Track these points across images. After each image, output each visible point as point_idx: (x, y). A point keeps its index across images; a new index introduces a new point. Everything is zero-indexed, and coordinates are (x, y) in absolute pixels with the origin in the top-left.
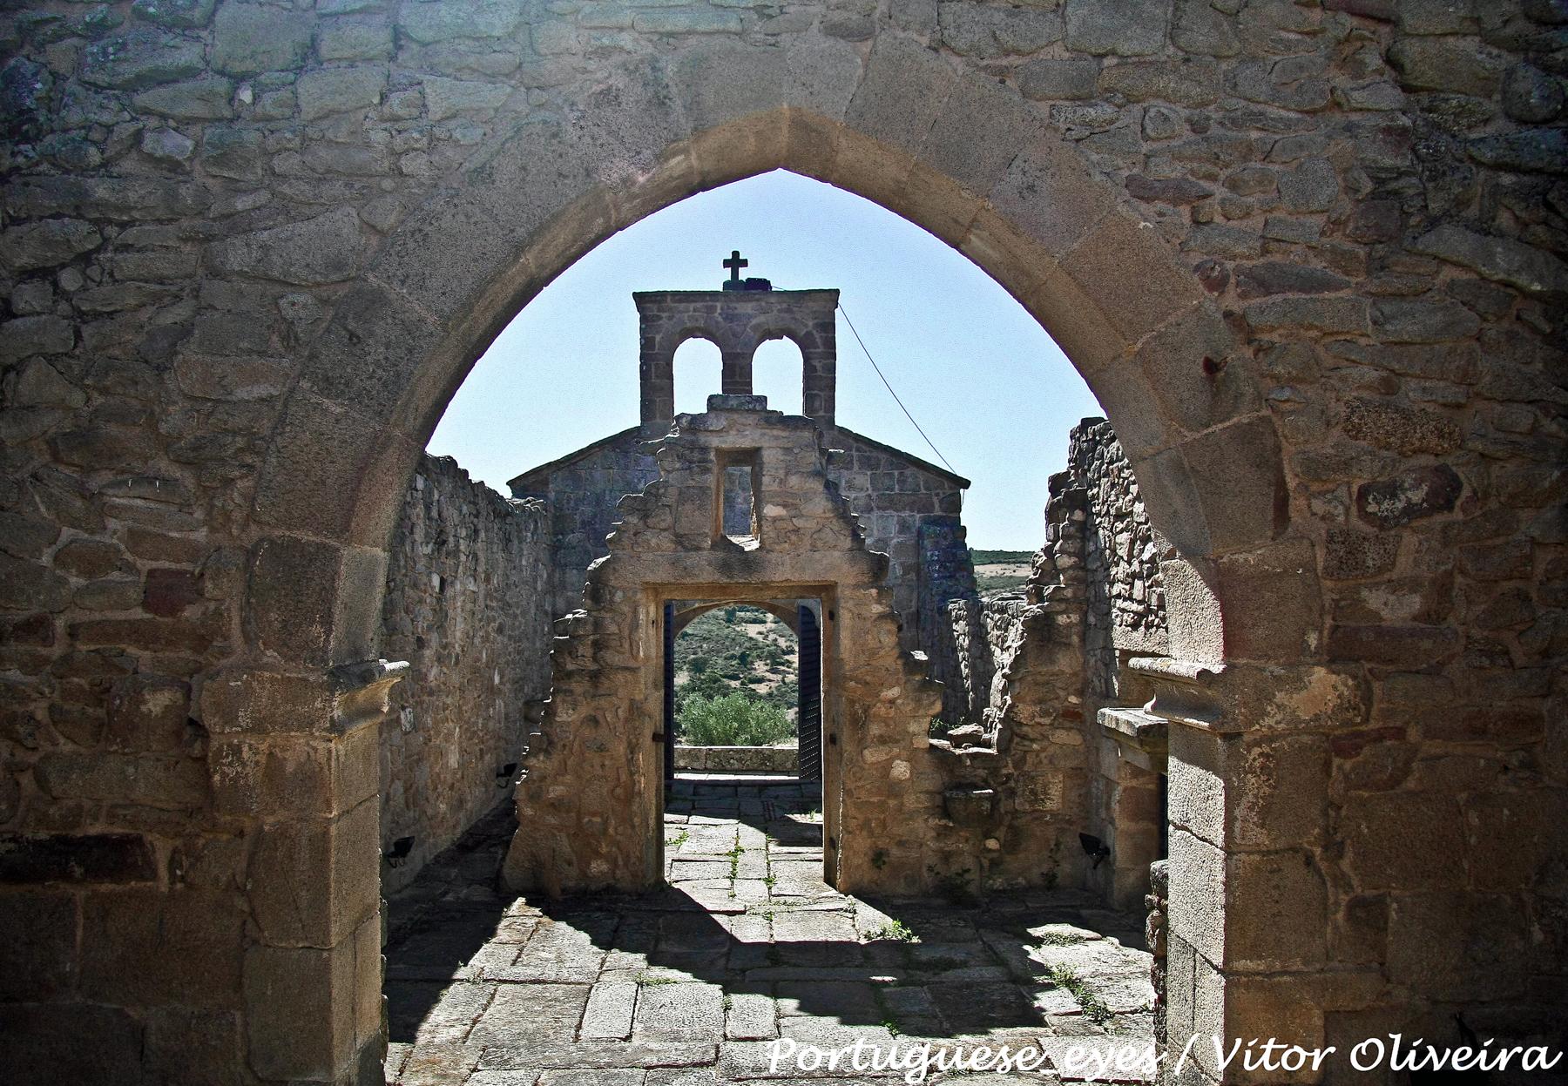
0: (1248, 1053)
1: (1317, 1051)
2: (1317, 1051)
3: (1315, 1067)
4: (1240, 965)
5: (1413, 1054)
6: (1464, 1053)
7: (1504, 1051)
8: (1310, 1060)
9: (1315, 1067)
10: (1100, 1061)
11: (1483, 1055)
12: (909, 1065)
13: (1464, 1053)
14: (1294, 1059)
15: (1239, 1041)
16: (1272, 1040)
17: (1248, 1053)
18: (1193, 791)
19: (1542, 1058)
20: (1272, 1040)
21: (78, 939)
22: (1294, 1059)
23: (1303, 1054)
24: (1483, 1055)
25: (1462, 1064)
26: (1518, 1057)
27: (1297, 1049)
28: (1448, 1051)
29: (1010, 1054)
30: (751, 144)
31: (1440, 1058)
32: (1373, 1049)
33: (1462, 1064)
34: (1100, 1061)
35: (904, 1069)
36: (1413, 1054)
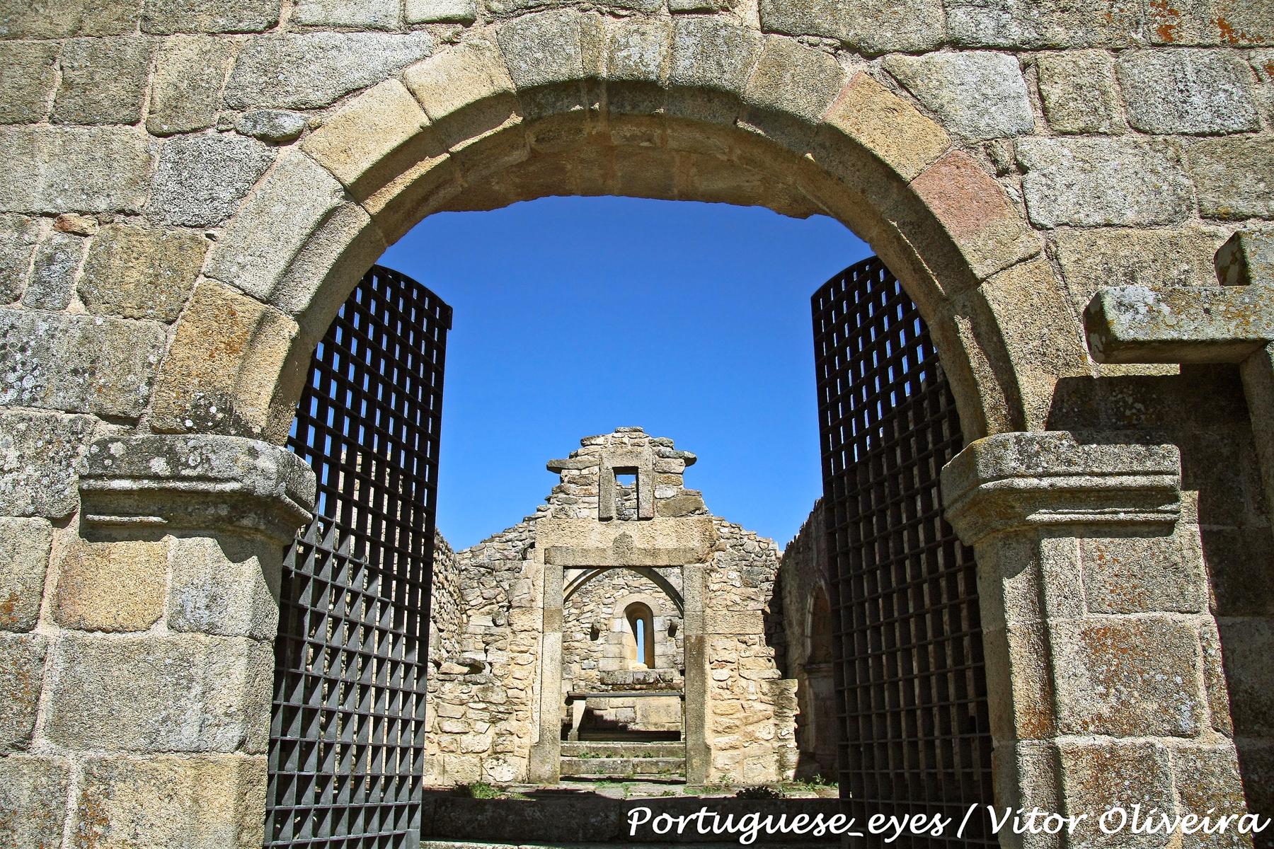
0: (1017, 819)
1: (682, 818)
2: (682, 818)
3: (680, 831)
4: (1012, 742)
5: (1149, 821)
6: (920, 819)
7: (1224, 818)
8: (675, 825)
9: (680, 831)
10: (1168, 825)
11: (1207, 821)
12: (743, 829)
13: (920, 819)
14: (663, 824)
15: (1009, 810)
16: (704, 809)
17: (1017, 819)
18: (964, 606)
19: (1254, 823)
20: (704, 809)
21: (1020, 705)
22: (663, 824)
23: (670, 820)
24: (1207, 821)
25: (917, 828)
26: (694, 822)
27: (665, 816)
28: (907, 817)
29: (825, 821)
30: (322, 240)
31: (1172, 824)
32: (1118, 817)
33: (917, 828)
34: (1168, 825)
35: (739, 833)
36: (1149, 821)
